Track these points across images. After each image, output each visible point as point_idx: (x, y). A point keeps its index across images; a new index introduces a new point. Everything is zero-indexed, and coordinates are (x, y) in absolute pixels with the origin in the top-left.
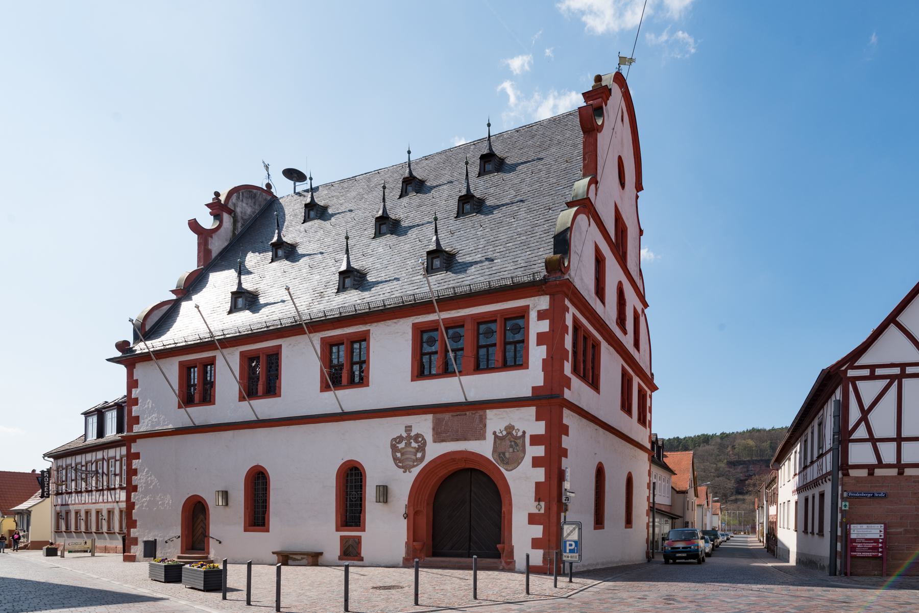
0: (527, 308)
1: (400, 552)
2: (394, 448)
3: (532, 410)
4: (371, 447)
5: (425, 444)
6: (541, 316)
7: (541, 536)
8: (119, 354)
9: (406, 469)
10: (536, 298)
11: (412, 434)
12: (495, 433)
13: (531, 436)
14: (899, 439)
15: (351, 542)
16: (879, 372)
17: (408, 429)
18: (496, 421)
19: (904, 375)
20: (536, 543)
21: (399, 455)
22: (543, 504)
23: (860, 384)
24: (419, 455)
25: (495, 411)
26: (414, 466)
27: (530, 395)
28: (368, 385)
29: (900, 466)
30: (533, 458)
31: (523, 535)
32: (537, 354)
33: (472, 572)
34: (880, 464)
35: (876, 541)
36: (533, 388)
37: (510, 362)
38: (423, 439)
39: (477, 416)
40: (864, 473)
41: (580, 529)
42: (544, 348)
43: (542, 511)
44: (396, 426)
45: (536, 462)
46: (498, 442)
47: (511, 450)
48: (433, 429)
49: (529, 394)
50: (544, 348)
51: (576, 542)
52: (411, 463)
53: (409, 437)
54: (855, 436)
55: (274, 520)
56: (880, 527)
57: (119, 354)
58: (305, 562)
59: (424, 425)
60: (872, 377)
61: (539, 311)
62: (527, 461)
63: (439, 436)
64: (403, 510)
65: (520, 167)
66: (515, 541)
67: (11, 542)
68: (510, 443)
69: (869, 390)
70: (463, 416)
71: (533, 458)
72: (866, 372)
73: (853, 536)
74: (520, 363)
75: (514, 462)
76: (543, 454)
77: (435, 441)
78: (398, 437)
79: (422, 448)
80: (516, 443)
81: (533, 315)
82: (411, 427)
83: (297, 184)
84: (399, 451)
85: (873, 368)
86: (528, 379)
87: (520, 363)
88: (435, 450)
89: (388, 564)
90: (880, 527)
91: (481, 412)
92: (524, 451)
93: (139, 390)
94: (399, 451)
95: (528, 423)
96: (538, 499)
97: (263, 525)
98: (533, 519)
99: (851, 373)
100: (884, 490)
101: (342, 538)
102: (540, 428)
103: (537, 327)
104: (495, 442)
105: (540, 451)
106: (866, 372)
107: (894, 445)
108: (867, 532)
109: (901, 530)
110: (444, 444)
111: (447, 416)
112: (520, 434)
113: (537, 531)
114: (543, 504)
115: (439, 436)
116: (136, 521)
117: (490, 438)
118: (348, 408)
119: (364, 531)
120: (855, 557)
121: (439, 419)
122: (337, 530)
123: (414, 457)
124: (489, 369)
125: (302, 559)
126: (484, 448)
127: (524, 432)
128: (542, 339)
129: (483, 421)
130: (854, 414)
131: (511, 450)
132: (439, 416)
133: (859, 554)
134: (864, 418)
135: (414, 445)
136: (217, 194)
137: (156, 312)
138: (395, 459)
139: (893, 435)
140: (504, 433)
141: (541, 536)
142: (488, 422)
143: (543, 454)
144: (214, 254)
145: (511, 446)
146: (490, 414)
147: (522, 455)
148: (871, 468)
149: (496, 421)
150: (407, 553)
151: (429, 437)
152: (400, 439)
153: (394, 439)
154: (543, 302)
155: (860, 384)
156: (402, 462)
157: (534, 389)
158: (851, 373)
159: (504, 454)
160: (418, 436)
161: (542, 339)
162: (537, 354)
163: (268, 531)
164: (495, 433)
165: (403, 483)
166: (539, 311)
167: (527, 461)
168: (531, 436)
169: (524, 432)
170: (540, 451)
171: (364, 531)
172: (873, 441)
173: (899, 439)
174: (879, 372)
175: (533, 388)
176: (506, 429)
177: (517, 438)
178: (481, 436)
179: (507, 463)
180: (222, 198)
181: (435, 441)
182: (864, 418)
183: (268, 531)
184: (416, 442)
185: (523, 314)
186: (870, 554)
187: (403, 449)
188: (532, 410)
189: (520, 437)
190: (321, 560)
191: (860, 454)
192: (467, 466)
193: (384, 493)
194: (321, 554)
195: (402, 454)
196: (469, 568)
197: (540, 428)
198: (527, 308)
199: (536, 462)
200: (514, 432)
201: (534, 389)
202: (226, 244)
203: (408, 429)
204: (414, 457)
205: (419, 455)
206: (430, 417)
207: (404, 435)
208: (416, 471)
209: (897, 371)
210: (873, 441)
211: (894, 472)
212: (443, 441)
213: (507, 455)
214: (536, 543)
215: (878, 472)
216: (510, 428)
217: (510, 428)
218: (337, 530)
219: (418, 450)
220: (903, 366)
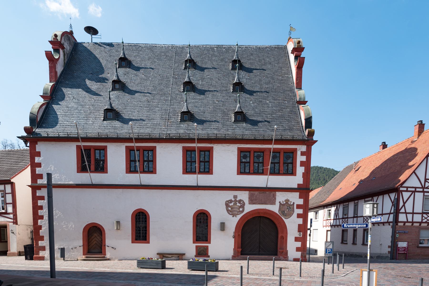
0: (296, 150)
1: (231, 253)
2: (227, 205)
3: (297, 194)
4: (215, 206)
5: (244, 204)
6: (302, 154)
7: (300, 246)
8: (25, 134)
9: (234, 215)
10: (300, 146)
11: (238, 199)
12: (280, 202)
13: (297, 205)
14: (413, 213)
15: (202, 249)
16: (409, 189)
17: (235, 197)
18: (281, 197)
19: (416, 191)
20: (298, 249)
21: (230, 209)
22: (301, 233)
23: (403, 193)
24: (241, 209)
25: (280, 193)
26: (238, 214)
27: (297, 187)
28: (212, 174)
29: (413, 222)
30: (298, 214)
31: (292, 246)
32: (300, 170)
33: (247, 261)
34: (408, 222)
35: (405, 248)
36: (298, 185)
37: (277, 171)
38: (243, 202)
39: (272, 194)
40: (418, 224)
41: (333, 244)
42: (303, 168)
43: (301, 236)
44: (229, 195)
45: (299, 216)
46: (281, 206)
47: (287, 210)
48: (249, 198)
49: (296, 187)
50: (303, 168)
51: (331, 249)
52: (237, 213)
53: (236, 201)
54: (401, 211)
55: (152, 237)
56: (406, 243)
57: (25, 134)
58: (173, 258)
59: (244, 196)
60: (407, 191)
61: (301, 152)
62: (295, 215)
63: (252, 201)
64: (232, 234)
65: (254, 71)
66: (289, 248)
67: (4, 253)
68: (287, 208)
69: (406, 195)
70: (269, 193)
71: (298, 214)
72: (405, 189)
73: (399, 246)
74: (293, 173)
75: (289, 215)
76: (302, 213)
77: (250, 204)
78: (229, 200)
79: (243, 206)
80: (290, 207)
81: (299, 153)
82: (237, 196)
83: (93, 36)
84: (230, 207)
85: (407, 188)
86: (297, 180)
87: (293, 173)
88: (249, 208)
89: (225, 258)
90: (406, 243)
91: (274, 193)
92: (294, 211)
93: (41, 159)
94: (230, 207)
95: (295, 199)
96: (299, 231)
97: (136, 240)
98: (297, 239)
99: (401, 189)
100: (407, 230)
101: (197, 247)
102: (301, 202)
103: (300, 158)
104: (280, 206)
105: (301, 211)
106: (405, 189)
107: (411, 215)
108: (402, 245)
109: (411, 244)
110: (254, 205)
111: (256, 193)
112: (292, 203)
113: (299, 244)
114: (301, 233)
115: (252, 201)
116: (43, 237)
117: (278, 204)
118: (200, 184)
119: (210, 243)
120: (399, 253)
121: (252, 194)
122: (194, 243)
123: (238, 210)
124: (279, 174)
125: (172, 257)
126: (275, 208)
127: (294, 203)
128: (302, 164)
129: (274, 196)
130: (401, 204)
131: (287, 210)
132: (252, 192)
133: (400, 252)
134: (404, 205)
135: (238, 204)
136: (56, 36)
137: (41, 109)
138: (228, 210)
139: (414, 212)
140: (285, 203)
141: (300, 246)
142: (277, 197)
143: (302, 213)
144: (58, 75)
145: (288, 208)
146: (278, 194)
147: (292, 213)
148: (405, 223)
149: (281, 197)
150: (234, 253)
151: (246, 201)
152: (231, 201)
153: (228, 201)
154: (303, 148)
155: (403, 193)
156: (231, 211)
157: (298, 185)
158: (401, 189)
159: (284, 211)
160: (240, 201)
161: (302, 164)
162: (300, 170)
163: (149, 243)
164: (280, 202)
165: (233, 222)
166: (301, 152)
167: (295, 215)
168: (297, 205)
169: (294, 203)
170: (301, 211)
171: (210, 243)
172: (406, 213)
173: (413, 213)
174: (409, 189)
175: (298, 185)
176: (285, 201)
177: (290, 205)
178: (273, 203)
179: (286, 216)
180: (59, 38)
181: (250, 204)
182: (404, 205)
183: (149, 243)
184: (240, 203)
185: (294, 152)
186: (403, 252)
187: (231, 207)
188: (297, 194)
189: (292, 205)
190: (184, 257)
191: (402, 218)
192: (265, 216)
193: (223, 226)
194: (184, 254)
195: (232, 209)
196: (272, 260)
197: (301, 202)
198: (296, 150)
199: (299, 216)
200: (289, 203)
201: (298, 185)
202: (62, 69)
203: (235, 197)
204: (238, 210)
205: (241, 209)
206: (247, 192)
207: (233, 199)
208: (239, 217)
209: (414, 189)
210: (406, 213)
211: (410, 224)
212: (254, 204)
213: (286, 212)
214: (298, 249)
215: (407, 224)
216: (287, 201)
217: (287, 201)
218: (194, 243)
219: (240, 207)
220: (416, 188)
